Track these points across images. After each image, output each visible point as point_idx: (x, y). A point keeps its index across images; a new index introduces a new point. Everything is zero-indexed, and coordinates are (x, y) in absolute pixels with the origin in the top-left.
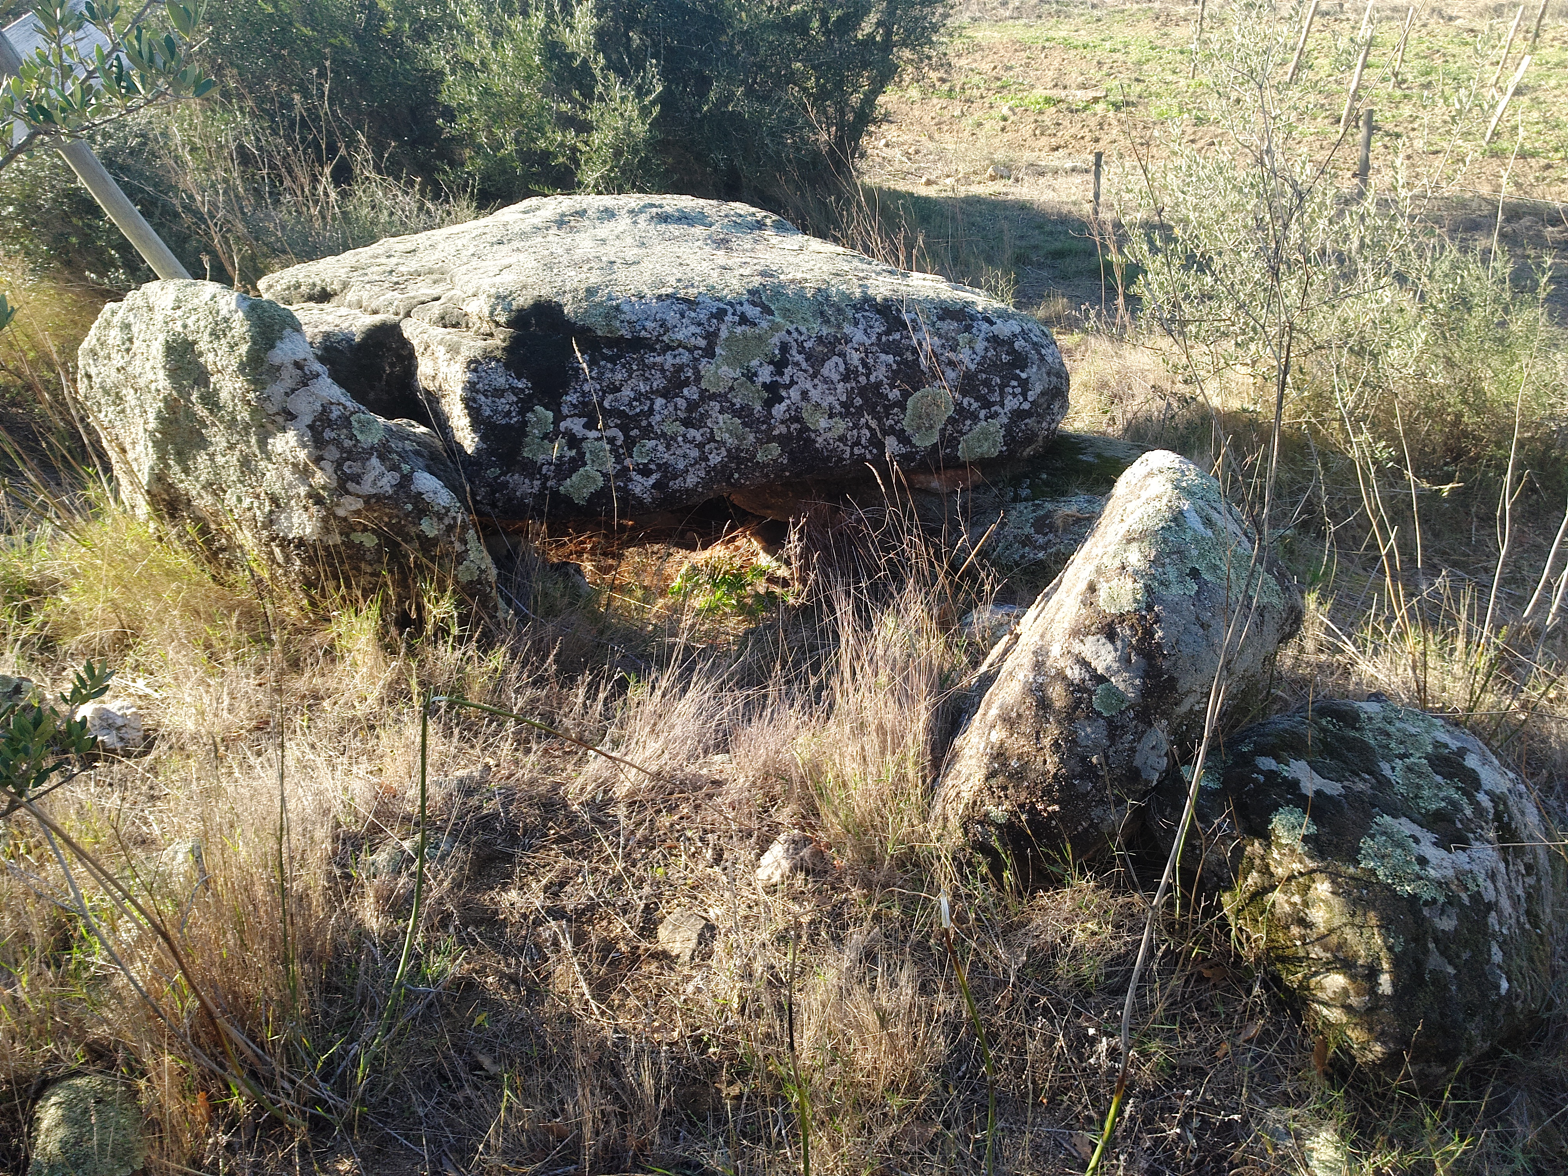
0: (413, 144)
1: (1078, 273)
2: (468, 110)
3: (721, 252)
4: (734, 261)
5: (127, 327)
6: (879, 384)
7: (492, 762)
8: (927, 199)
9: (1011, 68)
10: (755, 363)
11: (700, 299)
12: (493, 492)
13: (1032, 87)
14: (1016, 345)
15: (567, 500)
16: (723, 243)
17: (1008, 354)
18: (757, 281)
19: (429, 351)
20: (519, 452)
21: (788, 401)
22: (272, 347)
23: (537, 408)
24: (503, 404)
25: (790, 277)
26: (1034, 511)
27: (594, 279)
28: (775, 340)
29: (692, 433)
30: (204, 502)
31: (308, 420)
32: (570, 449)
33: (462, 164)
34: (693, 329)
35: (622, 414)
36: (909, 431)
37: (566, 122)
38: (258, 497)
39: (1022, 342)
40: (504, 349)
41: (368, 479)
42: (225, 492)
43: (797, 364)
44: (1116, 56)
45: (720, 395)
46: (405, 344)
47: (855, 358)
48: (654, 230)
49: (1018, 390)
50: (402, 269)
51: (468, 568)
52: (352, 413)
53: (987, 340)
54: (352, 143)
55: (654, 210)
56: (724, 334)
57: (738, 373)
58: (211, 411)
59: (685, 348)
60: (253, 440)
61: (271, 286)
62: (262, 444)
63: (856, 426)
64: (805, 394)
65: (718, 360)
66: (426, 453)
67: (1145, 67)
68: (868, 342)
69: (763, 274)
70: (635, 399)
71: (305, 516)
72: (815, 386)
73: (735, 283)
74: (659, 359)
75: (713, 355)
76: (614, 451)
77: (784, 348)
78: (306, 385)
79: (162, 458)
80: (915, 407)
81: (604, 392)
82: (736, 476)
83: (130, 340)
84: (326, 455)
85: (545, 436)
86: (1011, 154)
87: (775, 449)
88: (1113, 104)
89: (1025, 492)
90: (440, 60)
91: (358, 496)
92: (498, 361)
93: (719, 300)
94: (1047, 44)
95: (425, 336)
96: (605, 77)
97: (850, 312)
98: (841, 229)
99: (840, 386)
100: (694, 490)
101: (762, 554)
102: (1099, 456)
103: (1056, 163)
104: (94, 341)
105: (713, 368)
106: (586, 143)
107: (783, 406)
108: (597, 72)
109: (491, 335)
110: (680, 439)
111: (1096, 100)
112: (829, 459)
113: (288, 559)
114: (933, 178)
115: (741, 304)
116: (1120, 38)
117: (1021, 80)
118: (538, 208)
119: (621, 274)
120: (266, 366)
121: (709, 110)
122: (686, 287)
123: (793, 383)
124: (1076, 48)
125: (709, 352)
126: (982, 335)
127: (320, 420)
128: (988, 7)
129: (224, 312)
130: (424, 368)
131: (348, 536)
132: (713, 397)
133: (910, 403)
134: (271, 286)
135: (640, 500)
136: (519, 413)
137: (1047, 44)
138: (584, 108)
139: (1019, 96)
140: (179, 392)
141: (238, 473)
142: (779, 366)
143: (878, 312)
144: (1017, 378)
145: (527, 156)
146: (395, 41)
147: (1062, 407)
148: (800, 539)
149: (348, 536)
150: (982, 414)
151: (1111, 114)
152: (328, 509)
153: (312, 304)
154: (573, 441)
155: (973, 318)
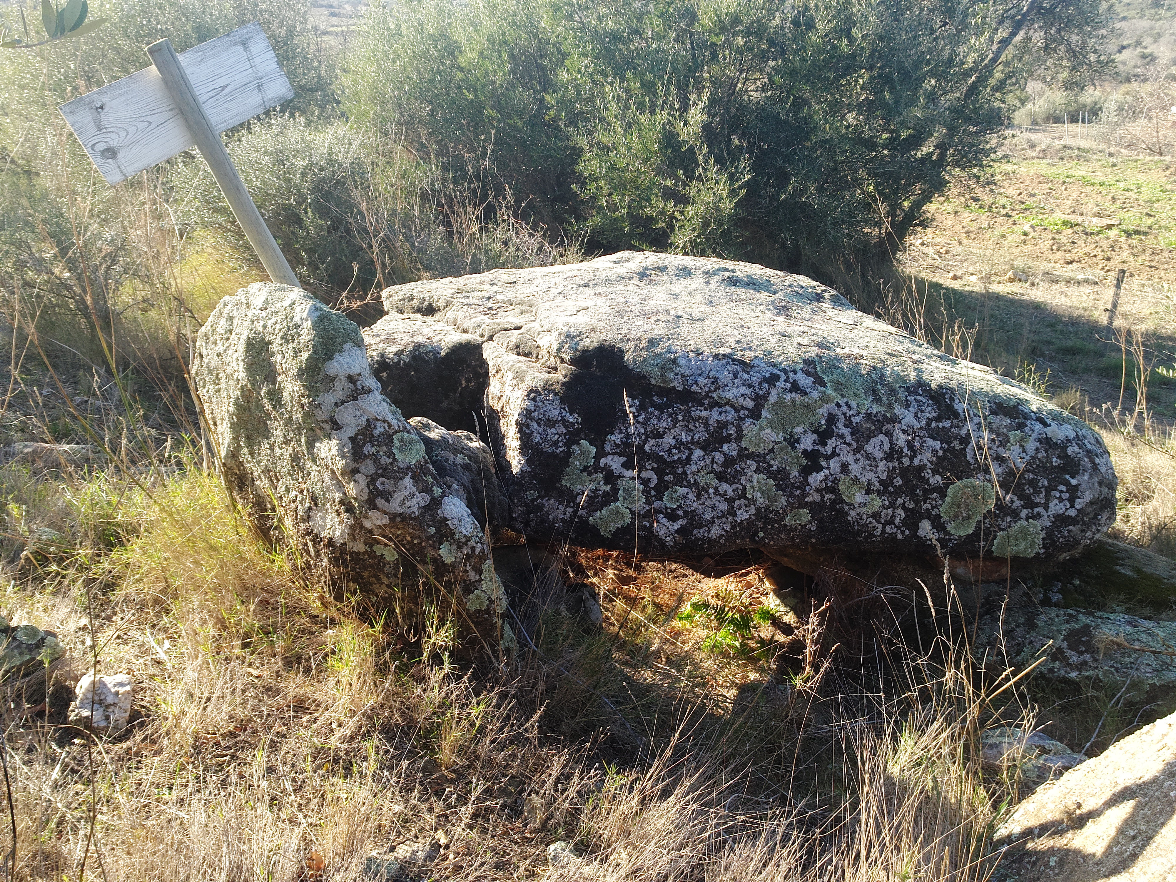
0: (554, 200)
1: (1088, 370)
2: (596, 179)
3: (781, 319)
4: (794, 328)
5: (231, 319)
6: (922, 468)
7: (443, 841)
8: (954, 291)
9: (1034, 195)
10: (799, 430)
11: (755, 362)
12: (529, 512)
13: (1052, 211)
14: (1070, 450)
15: (594, 530)
16: (783, 310)
17: (1059, 457)
18: (814, 352)
19: (500, 374)
20: (559, 480)
21: (826, 472)
22: (331, 358)
23: (583, 442)
24: (553, 433)
25: (846, 351)
26: (1068, 622)
27: (659, 331)
28: (824, 411)
29: (725, 487)
30: (263, 484)
31: (351, 433)
32: (606, 484)
33: (585, 220)
34: (743, 390)
35: (660, 459)
36: (945, 517)
37: (669, 194)
38: (302, 492)
39: (1076, 448)
40: (563, 384)
41: (398, 498)
42: (278, 480)
43: (842, 437)
44: (1128, 194)
45: (759, 455)
46: (483, 363)
47: (901, 439)
48: (722, 291)
49: (1066, 496)
50: (499, 297)
51: (478, 597)
52: (396, 432)
53: (1039, 440)
54: (500, 192)
55: (727, 274)
56: (773, 398)
57: (780, 437)
58: (274, 407)
59: (732, 406)
60: (303, 439)
61: (390, 296)
62: (310, 445)
63: (892, 505)
64: (845, 468)
65: (763, 422)
66: (474, 467)
67: (1155, 205)
68: (917, 425)
69: (820, 345)
70: (675, 447)
71: (337, 520)
72: (856, 461)
73: (792, 351)
74: (704, 414)
75: (758, 417)
76: (646, 492)
77: (831, 419)
78: (355, 399)
79: (236, 439)
80: (955, 496)
81: (647, 437)
82: (761, 534)
83: (231, 331)
84: (362, 469)
85: (585, 469)
86: (1030, 263)
87: (805, 515)
88: (1125, 232)
89: (1056, 597)
90: (583, 142)
91: (385, 513)
92: (556, 394)
93: (774, 365)
94: (1067, 180)
95: (499, 360)
96: (706, 162)
97: (903, 395)
98: (884, 307)
99: (882, 465)
100: (717, 541)
101: (771, 595)
102: (1138, 571)
103: (1070, 274)
104: (209, 328)
105: (756, 429)
106: (682, 213)
107: (821, 476)
108: (701, 159)
109: (556, 369)
110: (711, 491)
111: (1110, 227)
112: (859, 533)
113: (318, 554)
114: (959, 273)
115: (795, 372)
116: (1133, 180)
117: (1042, 205)
118: (628, 260)
119: (684, 329)
120: (321, 376)
121: (786, 198)
122: (744, 350)
123: (834, 454)
124: (1093, 185)
125: (755, 414)
126: (1035, 435)
127: (363, 434)
128: (1019, 148)
129: (297, 319)
130: (494, 388)
131: (371, 547)
132: (752, 456)
133: (950, 490)
134: (390, 296)
135: (662, 543)
136: (565, 444)
137: (1067, 180)
138: (685, 185)
139: (1040, 217)
140: (253, 385)
141: (289, 467)
142: (824, 436)
143: (932, 398)
144: (1067, 483)
145: (635, 219)
146: (554, 125)
147: (1109, 518)
148: (820, 624)
149: (371, 547)
150: (1024, 513)
151: (1123, 239)
152: (356, 519)
153: (419, 316)
154: (611, 477)
155: (1026, 416)
